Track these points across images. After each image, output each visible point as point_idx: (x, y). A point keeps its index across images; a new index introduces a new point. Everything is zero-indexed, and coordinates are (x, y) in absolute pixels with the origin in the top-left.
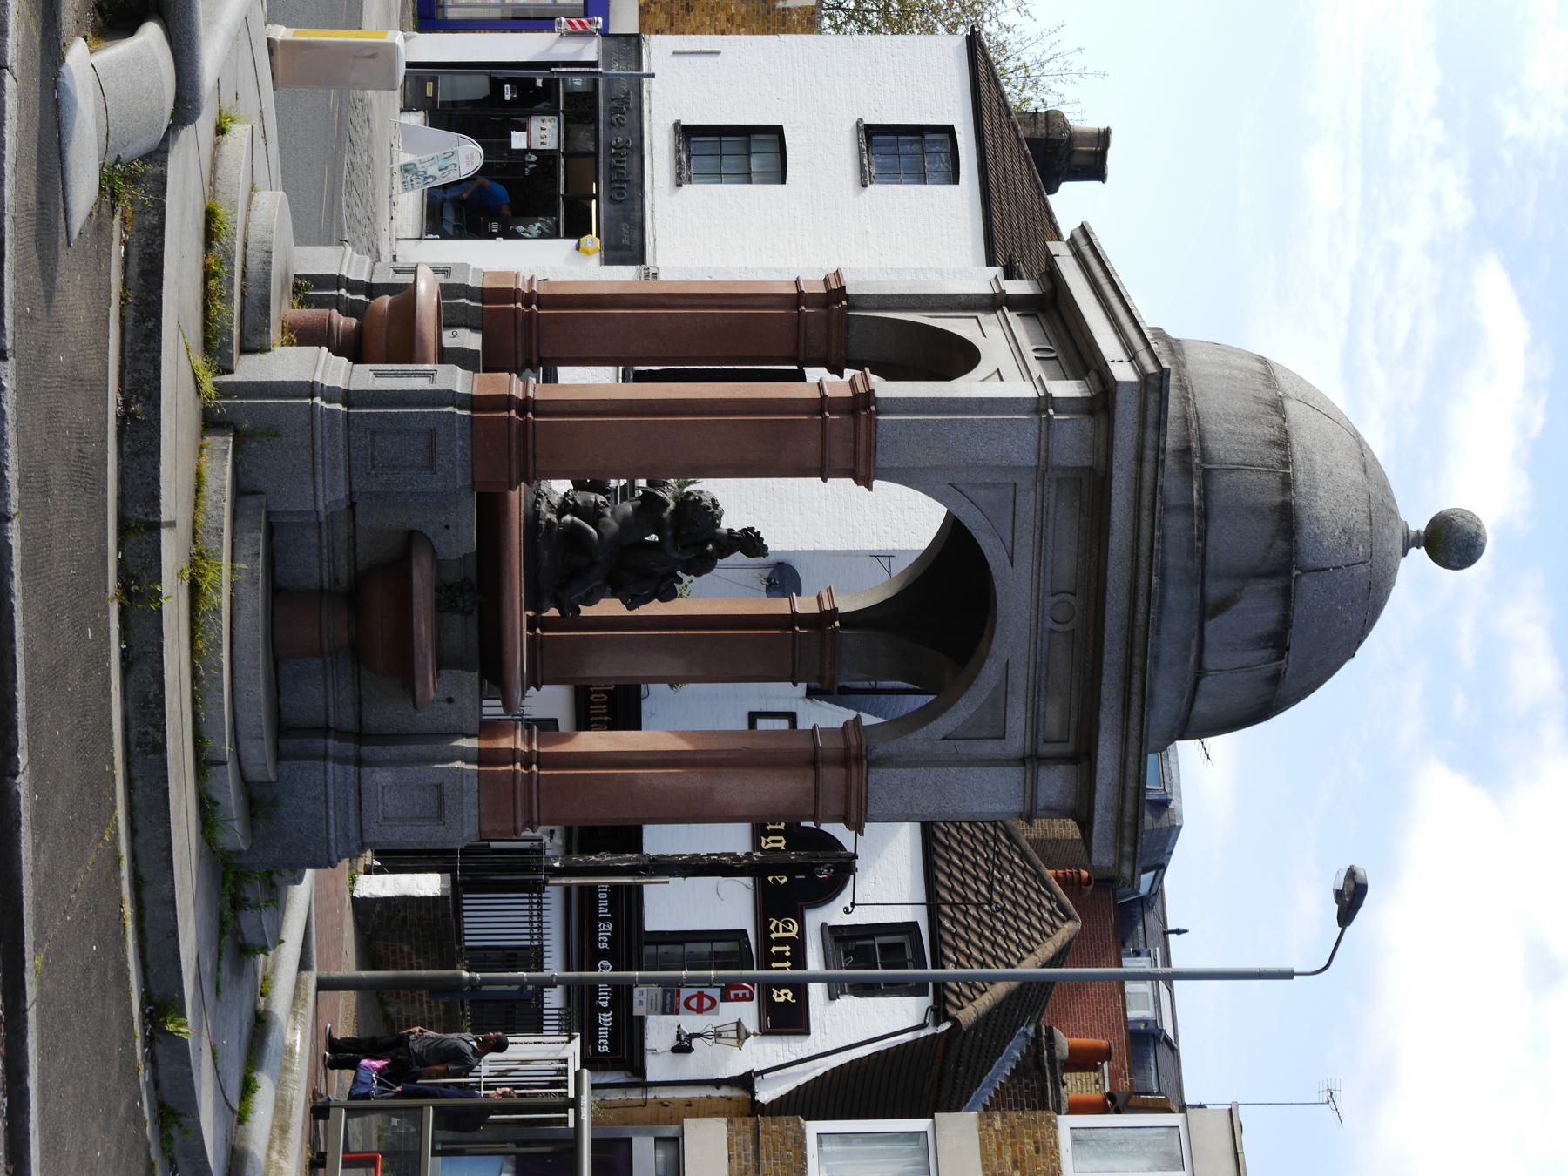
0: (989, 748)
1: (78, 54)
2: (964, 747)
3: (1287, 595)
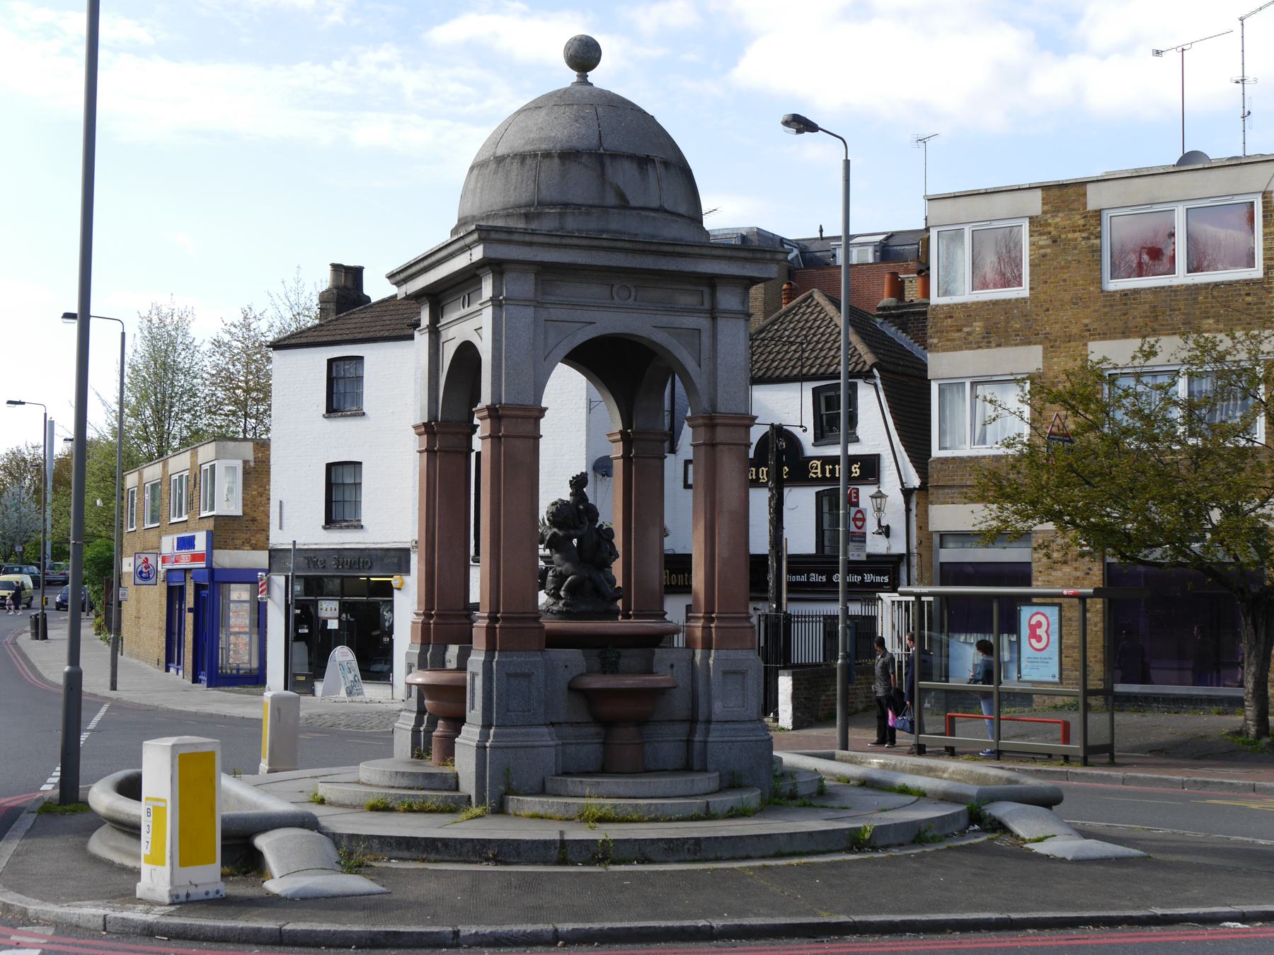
0: (706, 339)
1: (274, 886)
2: (705, 354)
3: (615, 156)
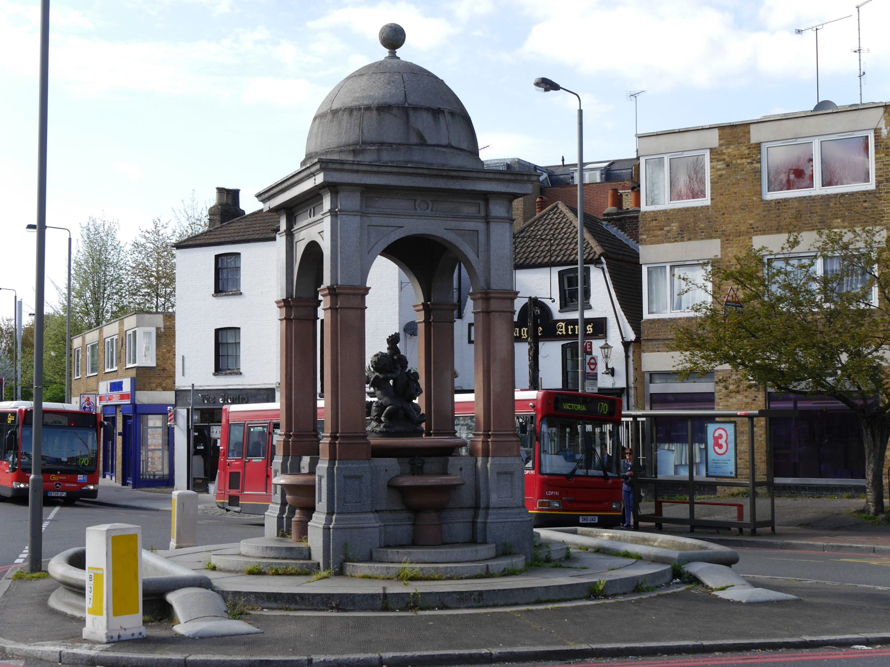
0: (482, 237)
1: (181, 629)
2: (482, 248)
3: (416, 109)
